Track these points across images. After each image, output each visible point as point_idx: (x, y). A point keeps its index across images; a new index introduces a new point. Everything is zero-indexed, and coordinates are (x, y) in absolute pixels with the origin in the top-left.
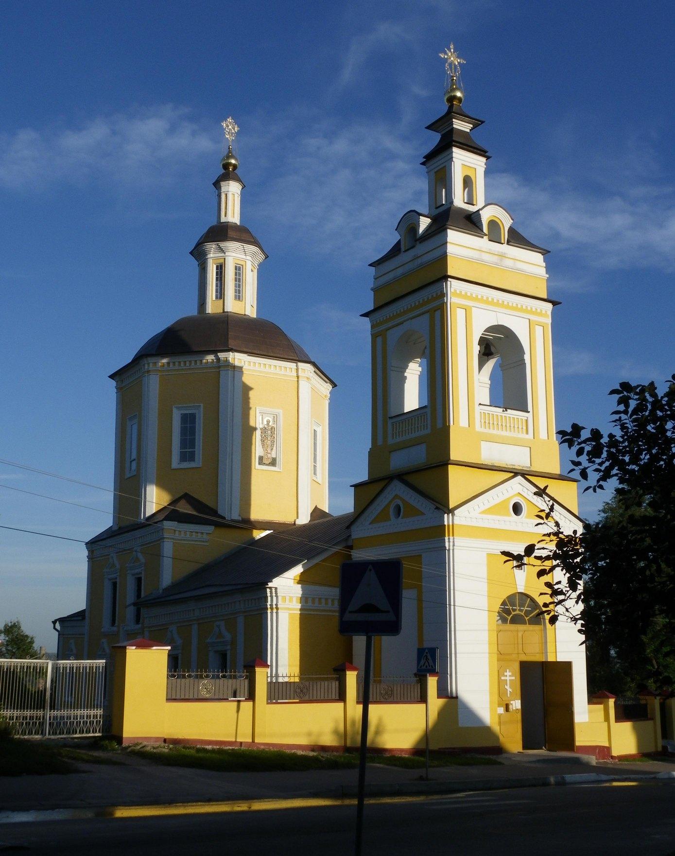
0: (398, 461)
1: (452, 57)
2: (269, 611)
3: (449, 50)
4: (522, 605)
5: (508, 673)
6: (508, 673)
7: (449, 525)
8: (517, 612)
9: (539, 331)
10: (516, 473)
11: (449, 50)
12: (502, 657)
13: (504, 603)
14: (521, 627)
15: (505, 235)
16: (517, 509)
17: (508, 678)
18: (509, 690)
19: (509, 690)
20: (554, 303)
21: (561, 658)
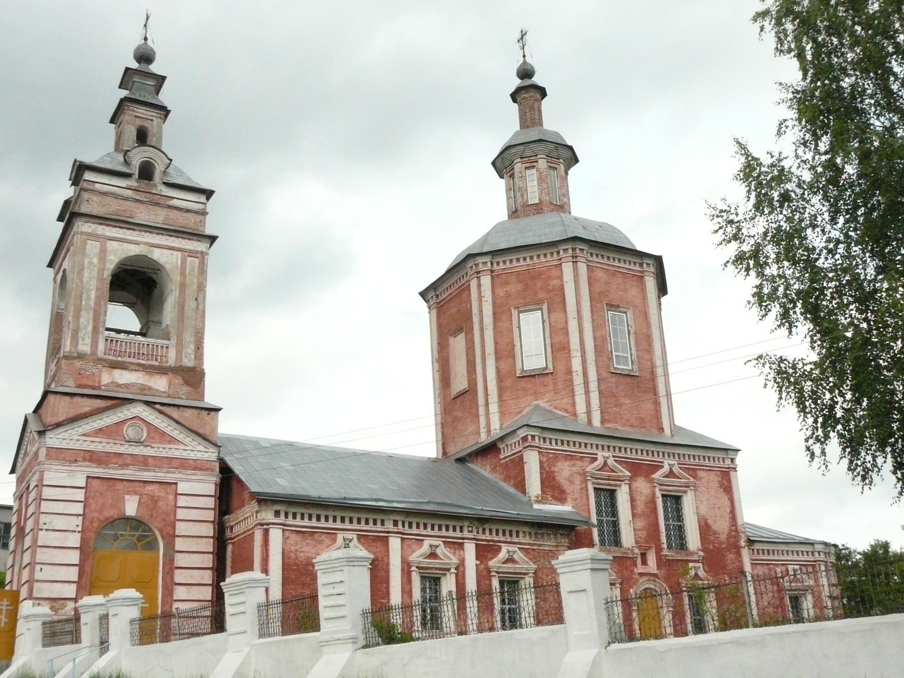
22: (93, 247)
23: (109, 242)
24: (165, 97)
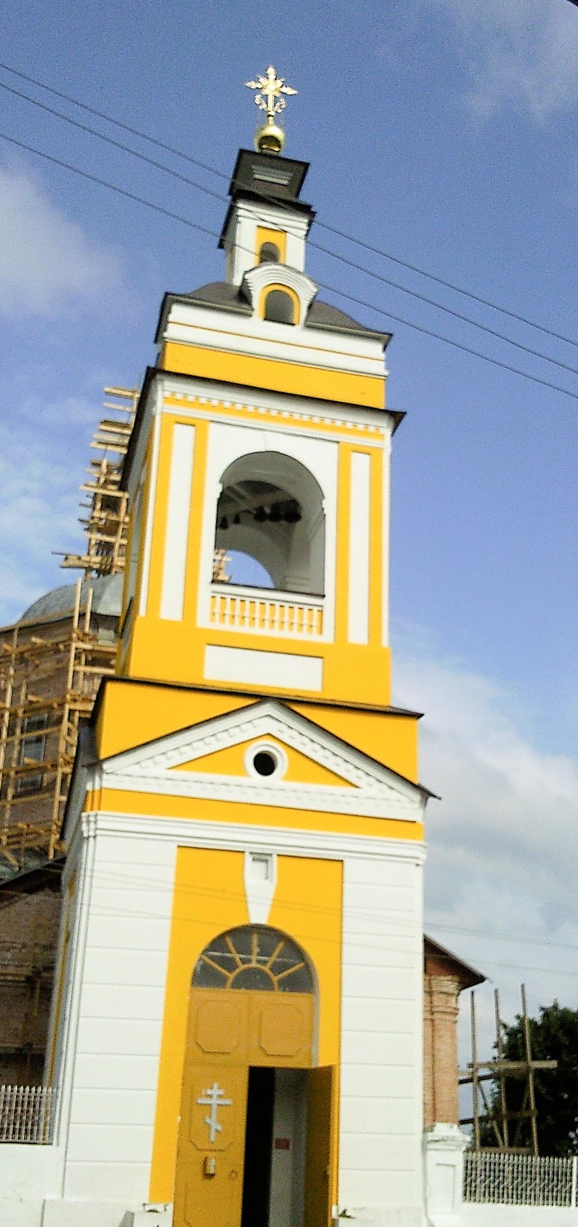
1: (271, 85)
2: (79, 906)
3: (267, 77)
4: (245, 949)
5: (216, 1091)
6: (216, 1091)
7: (93, 791)
8: (254, 965)
9: (360, 464)
10: (261, 698)
11: (267, 77)
12: (197, 1056)
13: (218, 943)
14: (261, 997)
15: (301, 312)
16: (265, 764)
17: (214, 1101)
18: (215, 1126)
19: (215, 1126)
20: (396, 417)
21: (321, 1064)
22: (183, 437)
23: (212, 425)
24: (312, 209)
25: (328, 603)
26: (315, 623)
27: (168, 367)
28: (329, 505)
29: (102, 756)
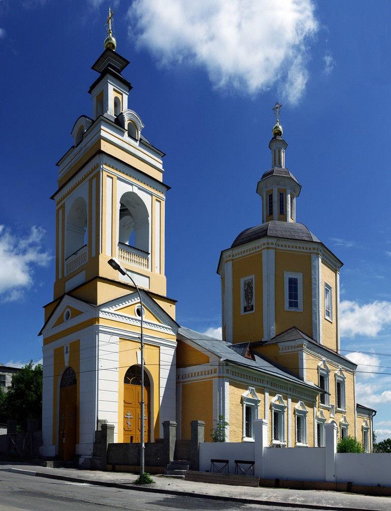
0: (70, 285)
17: (129, 417)
25: (150, 256)
26: (147, 264)
27: (100, 275)
28: (150, 219)
29: (99, 302)
